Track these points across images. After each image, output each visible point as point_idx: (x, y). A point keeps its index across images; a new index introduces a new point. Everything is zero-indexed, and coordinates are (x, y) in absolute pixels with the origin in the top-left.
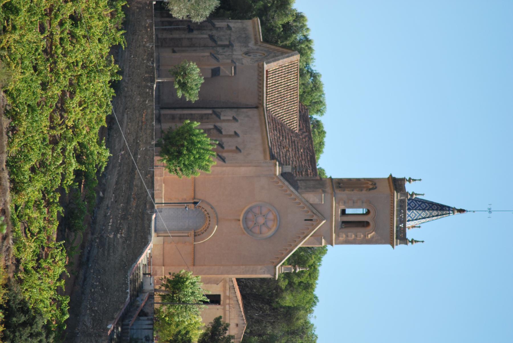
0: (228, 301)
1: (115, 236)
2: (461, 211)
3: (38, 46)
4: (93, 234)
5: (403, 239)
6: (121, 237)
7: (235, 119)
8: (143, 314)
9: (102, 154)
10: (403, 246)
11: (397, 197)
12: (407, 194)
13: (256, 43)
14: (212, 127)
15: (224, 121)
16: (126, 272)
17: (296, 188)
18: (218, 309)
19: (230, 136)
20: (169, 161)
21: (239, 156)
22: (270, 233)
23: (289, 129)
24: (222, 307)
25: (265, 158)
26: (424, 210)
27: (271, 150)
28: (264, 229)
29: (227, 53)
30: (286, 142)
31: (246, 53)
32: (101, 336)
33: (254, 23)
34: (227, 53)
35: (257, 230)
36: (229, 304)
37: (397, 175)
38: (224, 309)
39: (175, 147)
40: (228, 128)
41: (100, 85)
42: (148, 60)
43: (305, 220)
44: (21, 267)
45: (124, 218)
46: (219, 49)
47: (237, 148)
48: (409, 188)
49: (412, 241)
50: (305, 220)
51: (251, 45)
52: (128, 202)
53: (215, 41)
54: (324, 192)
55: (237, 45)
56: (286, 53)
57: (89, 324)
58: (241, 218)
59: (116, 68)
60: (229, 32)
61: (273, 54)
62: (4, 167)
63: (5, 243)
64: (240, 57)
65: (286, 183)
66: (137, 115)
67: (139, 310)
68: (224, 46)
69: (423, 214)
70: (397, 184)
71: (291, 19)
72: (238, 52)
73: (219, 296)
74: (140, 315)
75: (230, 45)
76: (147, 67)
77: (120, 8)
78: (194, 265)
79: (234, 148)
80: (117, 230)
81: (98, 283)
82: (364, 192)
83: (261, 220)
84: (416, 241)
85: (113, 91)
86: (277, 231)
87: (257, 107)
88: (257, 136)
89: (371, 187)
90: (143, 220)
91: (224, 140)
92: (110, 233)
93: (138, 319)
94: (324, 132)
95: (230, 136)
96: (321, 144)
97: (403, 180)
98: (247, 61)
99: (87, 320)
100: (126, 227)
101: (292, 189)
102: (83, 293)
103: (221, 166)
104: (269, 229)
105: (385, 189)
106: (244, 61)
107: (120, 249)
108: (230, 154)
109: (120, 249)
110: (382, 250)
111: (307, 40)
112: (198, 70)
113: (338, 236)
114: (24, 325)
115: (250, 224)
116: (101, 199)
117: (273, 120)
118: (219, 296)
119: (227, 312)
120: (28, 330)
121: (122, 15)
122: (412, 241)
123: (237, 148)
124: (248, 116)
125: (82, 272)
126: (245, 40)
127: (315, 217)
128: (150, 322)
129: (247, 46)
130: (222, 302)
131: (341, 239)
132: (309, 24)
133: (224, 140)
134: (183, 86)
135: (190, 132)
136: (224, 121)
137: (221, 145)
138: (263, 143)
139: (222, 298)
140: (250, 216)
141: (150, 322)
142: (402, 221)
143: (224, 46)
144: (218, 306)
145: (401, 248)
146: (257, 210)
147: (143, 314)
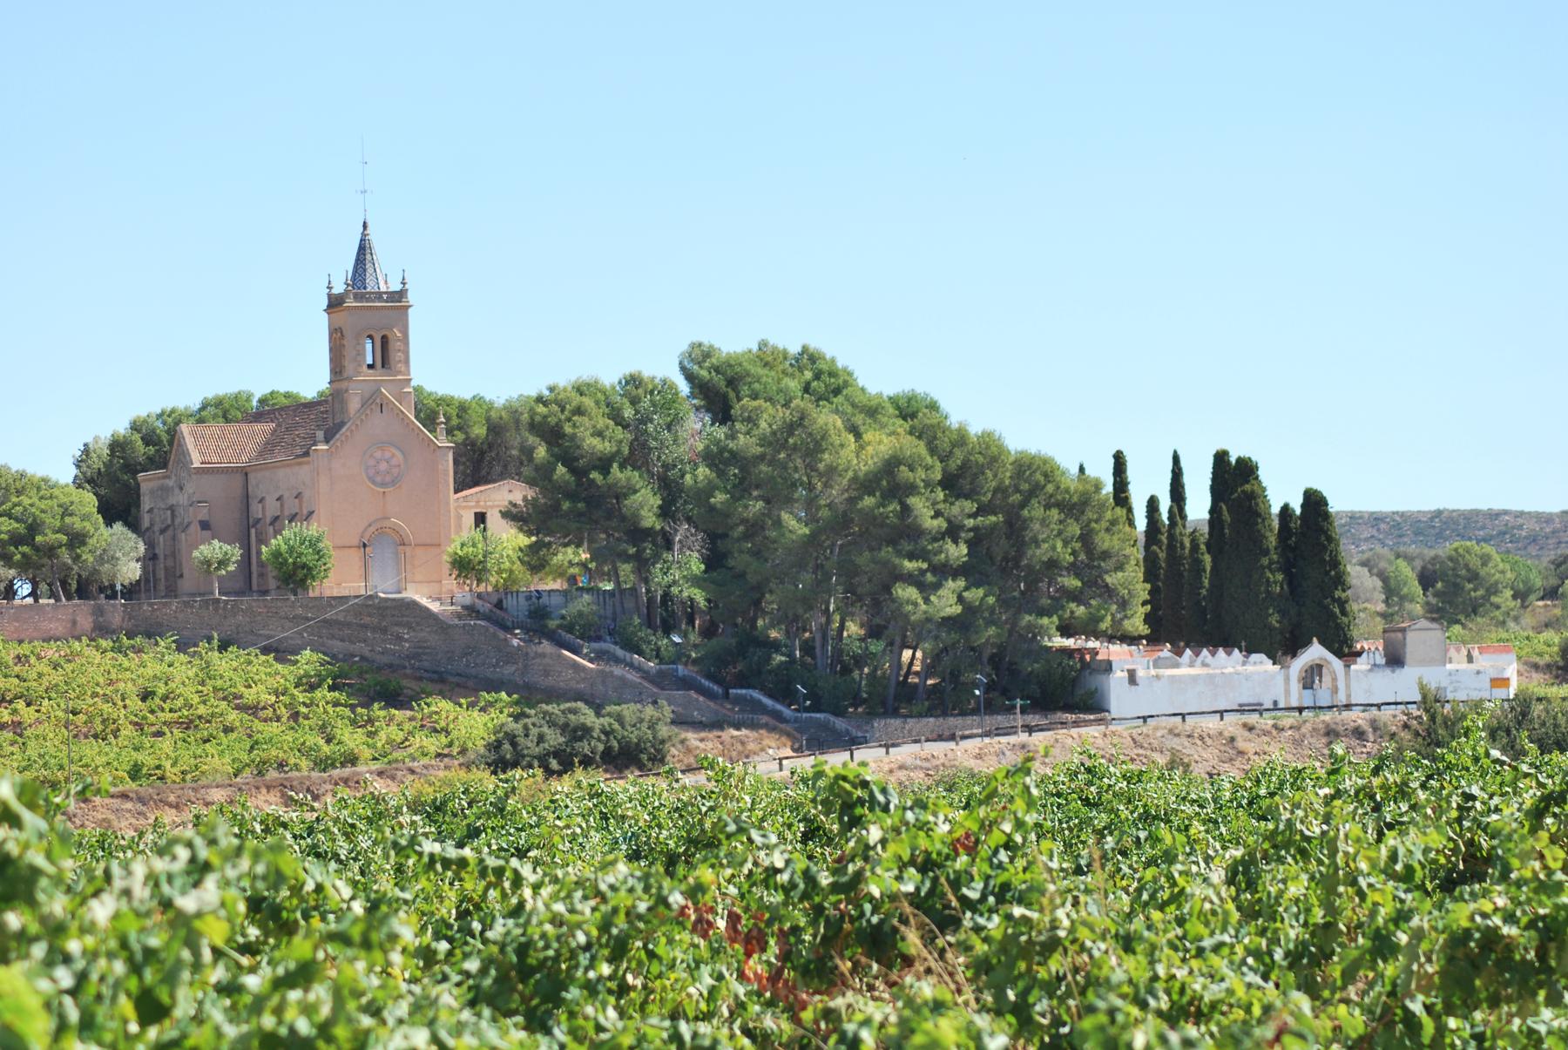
2: (365, 226)
5: (401, 295)
8: (499, 605)
9: (308, 660)
11: (350, 303)
17: (342, 424)
21: (307, 494)
22: (398, 454)
28: (394, 462)
35: (395, 471)
41: (225, 664)
45: (384, 631)
46: (178, 521)
48: (339, 288)
51: (170, 483)
52: (365, 626)
53: (168, 527)
55: (172, 501)
69: (370, 270)
70: (335, 303)
74: (501, 608)
75: (172, 508)
80: (399, 638)
88: (281, 473)
91: (286, 513)
93: (506, 610)
96: (287, 395)
97: (330, 296)
98: (190, 488)
99: (509, 670)
105: (341, 318)
113: (400, 373)
114: (514, 744)
116: (363, 658)
117: (261, 454)
120: (521, 740)
125: (452, 679)
126: (165, 490)
133: (286, 513)
140: (378, 479)
142: (379, 296)
145: (412, 297)
146: (371, 472)
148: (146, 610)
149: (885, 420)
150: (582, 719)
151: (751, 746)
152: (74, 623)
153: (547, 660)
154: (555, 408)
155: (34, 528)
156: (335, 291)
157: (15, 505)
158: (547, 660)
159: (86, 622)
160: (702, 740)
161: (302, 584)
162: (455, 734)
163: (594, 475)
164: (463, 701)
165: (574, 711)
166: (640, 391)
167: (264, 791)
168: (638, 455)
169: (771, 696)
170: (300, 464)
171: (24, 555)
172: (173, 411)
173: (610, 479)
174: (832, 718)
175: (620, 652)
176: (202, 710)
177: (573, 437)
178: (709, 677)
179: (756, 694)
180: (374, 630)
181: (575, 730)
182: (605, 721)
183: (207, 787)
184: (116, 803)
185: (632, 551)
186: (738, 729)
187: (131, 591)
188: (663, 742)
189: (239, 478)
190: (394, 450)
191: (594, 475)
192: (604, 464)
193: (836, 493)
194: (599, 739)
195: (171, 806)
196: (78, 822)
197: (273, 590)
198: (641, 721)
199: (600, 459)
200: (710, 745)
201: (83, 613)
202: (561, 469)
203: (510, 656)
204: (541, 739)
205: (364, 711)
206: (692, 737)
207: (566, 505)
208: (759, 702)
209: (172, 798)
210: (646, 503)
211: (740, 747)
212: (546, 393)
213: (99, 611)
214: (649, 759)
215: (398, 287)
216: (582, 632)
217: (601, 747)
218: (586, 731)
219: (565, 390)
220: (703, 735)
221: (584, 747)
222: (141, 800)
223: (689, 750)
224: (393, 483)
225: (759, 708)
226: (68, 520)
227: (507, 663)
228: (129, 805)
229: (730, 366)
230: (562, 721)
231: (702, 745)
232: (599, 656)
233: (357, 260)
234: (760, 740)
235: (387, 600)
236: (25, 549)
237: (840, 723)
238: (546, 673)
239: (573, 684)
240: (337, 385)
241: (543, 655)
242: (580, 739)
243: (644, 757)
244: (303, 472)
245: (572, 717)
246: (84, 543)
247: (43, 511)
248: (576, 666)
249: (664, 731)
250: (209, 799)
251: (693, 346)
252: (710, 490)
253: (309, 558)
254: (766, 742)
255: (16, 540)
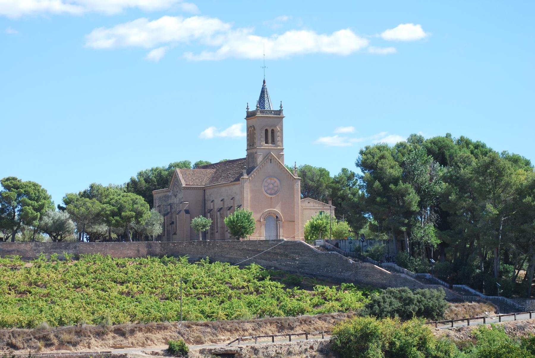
1: (297, 260)
2: (264, 82)
4: (296, 272)
5: (279, 112)
6: (298, 257)
7: (213, 201)
8: (337, 245)
9: (255, 267)
10: (284, 112)
11: (259, 114)
12: (257, 110)
13: (169, 191)
14: (219, 213)
15: (214, 207)
16: (319, 254)
17: (253, 168)
19: (224, 203)
20: (247, 234)
21: (237, 198)
22: (277, 181)
23: (215, 174)
25: (239, 184)
26: (264, 101)
27: (232, 182)
28: (276, 184)
29: (176, 206)
30: (225, 175)
31: (176, 196)
32: (357, 267)
33: (155, 194)
34: (176, 206)
35: (276, 188)
37: (245, 115)
39: (239, 230)
40: (218, 204)
41: (217, 268)
42: (193, 244)
44: (341, 309)
45: (287, 256)
46: (173, 211)
47: (232, 199)
48: (253, 108)
49: (281, 107)
51: (169, 194)
52: (278, 254)
53: (168, 213)
54: (256, 153)
55: (170, 201)
56: (175, 175)
57: (350, 273)
58: (270, 196)
59: (202, 261)
60: (162, 206)
61: (176, 183)
62: (296, 317)
63: (336, 317)
64: (178, 199)
65: (252, 172)
66: (225, 250)
67: (335, 247)
68: (171, 208)
69: (266, 101)
70: (250, 115)
71: (142, 179)
72: (175, 200)
74: (338, 247)
75: (170, 205)
76: (197, 245)
77: (168, 259)
79: (232, 201)
80: (294, 259)
82: (256, 132)
83: (271, 186)
85: (217, 262)
86: (275, 177)
87: (205, 191)
88: (223, 189)
89: (253, 128)
90: (288, 245)
91: (226, 206)
92: (296, 263)
93: (340, 248)
94: (200, 161)
95: (224, 203)
96: (206, 162)
97: (247, 112)
98: (180, 196)
99: (347, 274)
100: (292, 255)
101: (255, 170)
102: (331, 277)
103: (244, 206)
104: (275, 182)
105: (253, 121)
106: (181, 197)
107: (305, 257)
108: (235, 203)
109: (305, 257)
110: (285, 122)
111: (152, 170)
112: (196, 218)
113: (279, 146)
114: (379, 306)
115: (273, 192)
116: (276, 268)
117: (211, 182)
120: (382, 304)
121: (172, 258)
122: (281, 107)
123: (232, 199)
124: (210, 195)
125: (320, 278)
126: (167, 197)
127: (270, 158)
128: (341, 242)
129: (171, 196)
131: (280, 144)
132: (144, 170)
133: (226, 206)
134: (204, 226)
135: (231, 222)
136: (214, 207)
137: (230, 208)
138: (227, 186)
140: (269, 192)
141: (341, 242)
142: (271, 112)
143: (171, 208)
145: (284, 113)
146: (266, 188)
147: (337, 245)
148: (167, 246)
149: (521, 165)
150: (409, 295)
151: (478, 310)
152: (138, 251)
153: (367, 270)
154: (369, 156)
155: (121, 209)
156: (250, 110)
157: (111, 199)
158: (367, 270)
159: (144, 250)
160: (457, 307)
161: (242, 235)
162: (344, 301)
163: (392, 186)
164: (334, 287)
165: (404, 291)
166: (405, 150)
167: (269, 325)
168: (407, 177)
169: (472, 287)
170: (234, 184)
171: (116, 221)
172: (157, 169)
173: (398, 187)
174: (506, 299)
175: (397, 267)
176: (215, 288)
177: (381, 169)
178: (439, 278)
179: (467, 288)
180: (281, 255)
181: (405, 300)
182: (419, 296)
183: (244, 322)
184: (203, 329)
185: (406, 221)
186: (471, 302)
187: (159, 238)
188: (442, 307)
189: (201, 192)
190: (275, 179)
191: (392, 186)
192: (395, 181)
193: (508, 197)
194: (416, 305)
195: (228, 331)
196: (186, 338)
197: (225, 240)
198: (433, 297)
199: (393, 179)
200: (460, 309)
201: (142, 247)
202: (377, 183)
203: (349, 268)
204: (391, 304)
205: (290, 290)
206: (453, 305)
207: (378, 199)
208: (468, 291)
209: (228, 327)
210: (413, 198)
211: (473, 310)
212: (364, 149)
213: (149, 246)
214: (436, 315)
215: (279, 109)
216: (377, 258)
217: (417, 309)
218: (410, 301)
219: (373, 149)
220: (456, 304)
221: (411, 308)
222: (214, 327)
223: (452, 311)
224: (275, 194)
225: (468, 293)
226: (135, 206)
227: (347, 270)
228: (209, 330)
229: (440, 142)
230: (399, 296)
231: (457, 309)
232: (388, 268)
233: (261, 94)
234: (481, 308)
235: (287, 242)
236: (117, 218)
237: (510, 301)
238: (367, 276)
239: (380, 281)
240: (251, 151)
241: (365, 267)
242: (408, 304)
243: (435, 314)
244: (235, 188)
245: (403, 294)
246: (141, 217)
247: (125, 202)
248: (381, 272)
249: (443, 302)
250: (245, 328)
251: (412, 136)
252: (447, 194)
253: (246, 224)
254: (484, 308)
255: (113, 214)
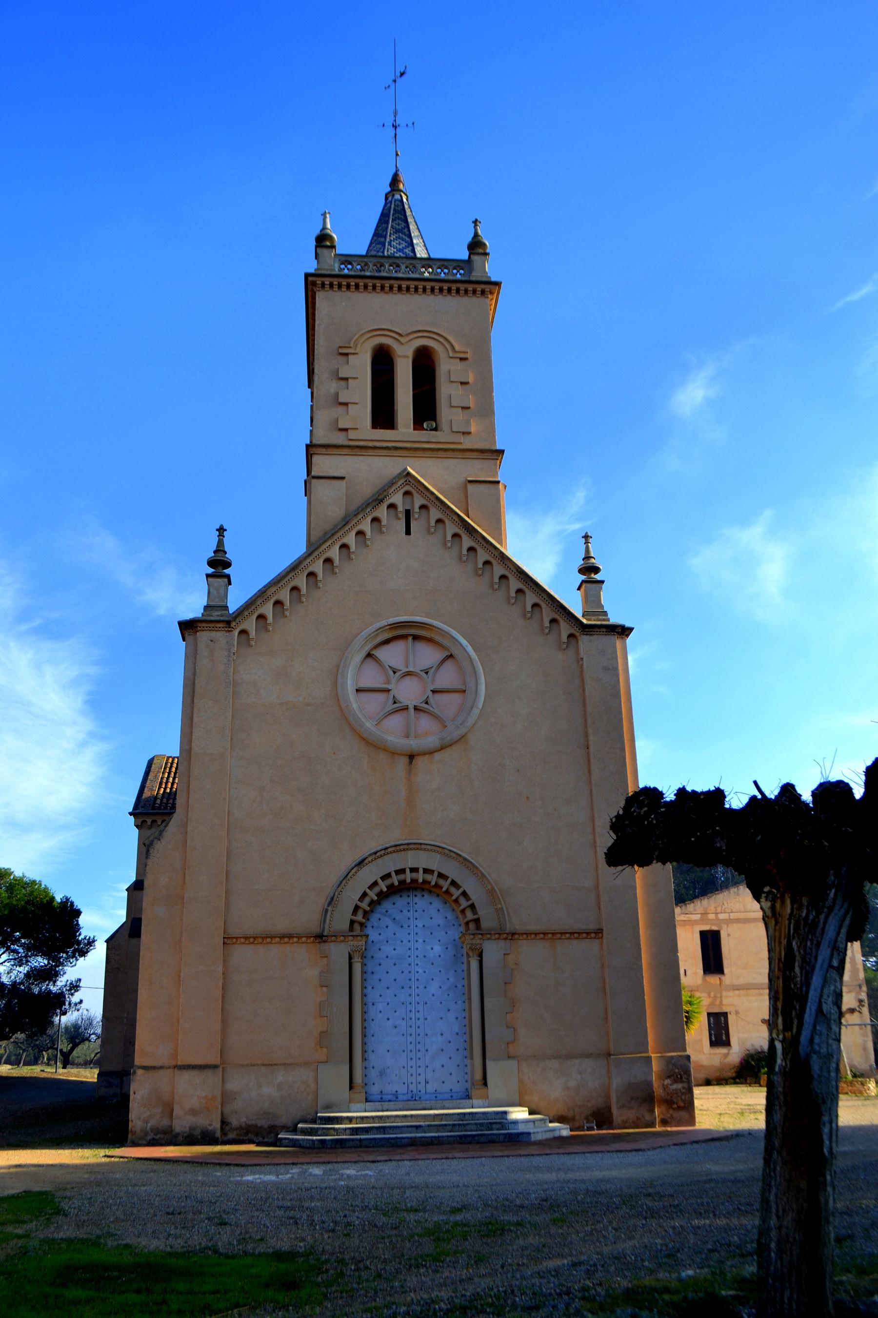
0: (711, 916)
3: (545, 1304)
18: (729, 935)
24: (724, 926)
36: (716, 913)
38: (728, 922)
43: (408, 532)
50: (408, 532)
73: (703, 934)
74: (427, 703)
78: (357, 690)
81: (319, 1279)
84: (587, 542)
118: (703, 934)
119: (733, 916)
130: (715, 928)
139: (706, 928)
144: (723, 935)
